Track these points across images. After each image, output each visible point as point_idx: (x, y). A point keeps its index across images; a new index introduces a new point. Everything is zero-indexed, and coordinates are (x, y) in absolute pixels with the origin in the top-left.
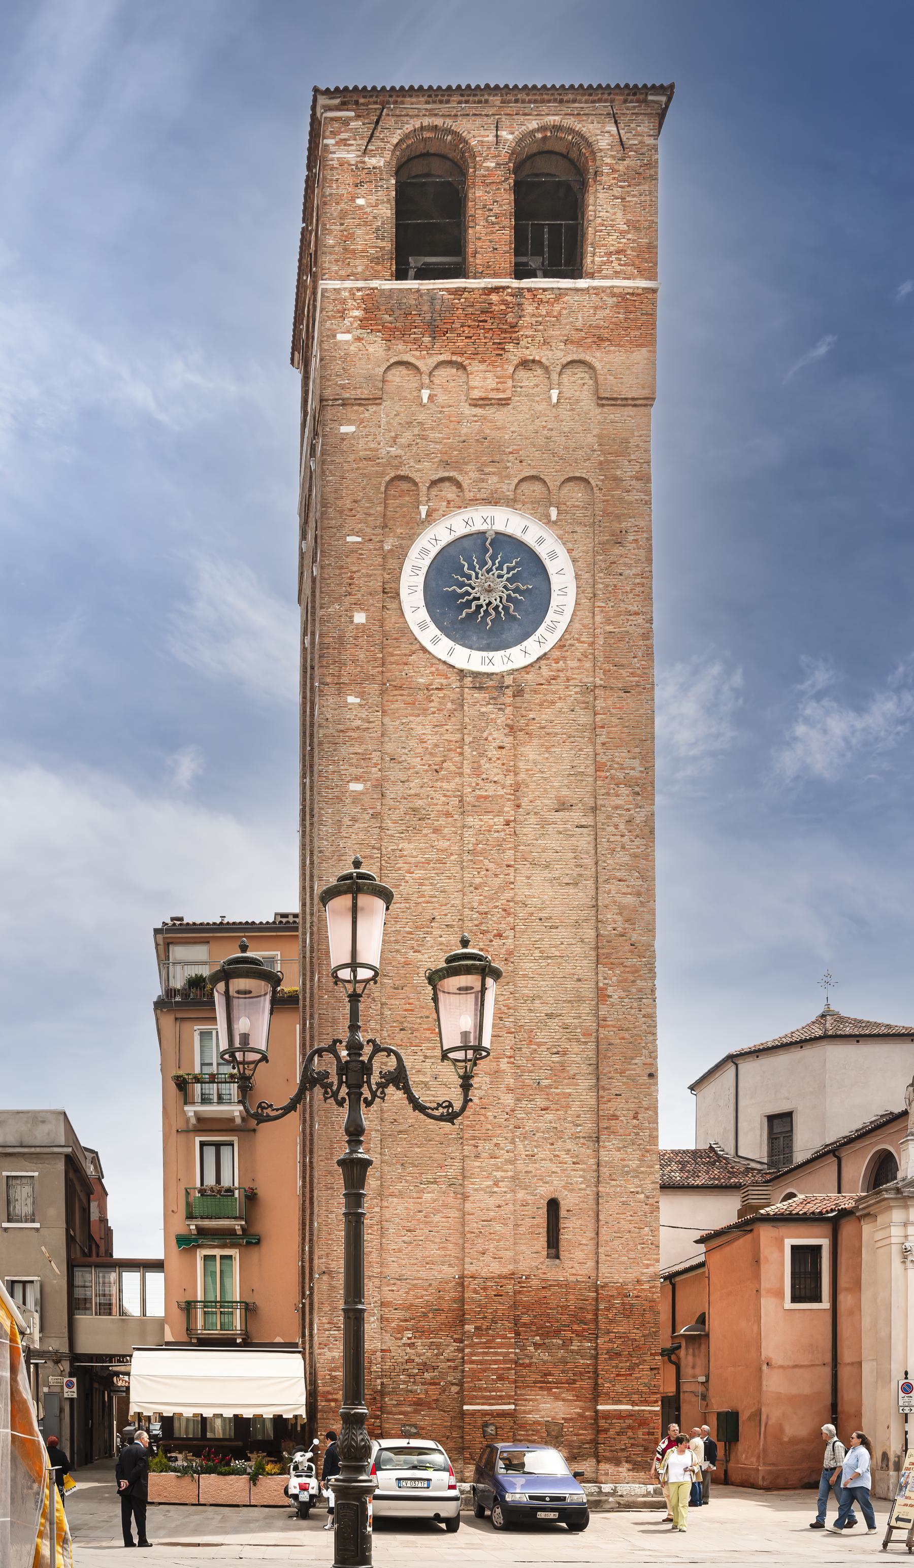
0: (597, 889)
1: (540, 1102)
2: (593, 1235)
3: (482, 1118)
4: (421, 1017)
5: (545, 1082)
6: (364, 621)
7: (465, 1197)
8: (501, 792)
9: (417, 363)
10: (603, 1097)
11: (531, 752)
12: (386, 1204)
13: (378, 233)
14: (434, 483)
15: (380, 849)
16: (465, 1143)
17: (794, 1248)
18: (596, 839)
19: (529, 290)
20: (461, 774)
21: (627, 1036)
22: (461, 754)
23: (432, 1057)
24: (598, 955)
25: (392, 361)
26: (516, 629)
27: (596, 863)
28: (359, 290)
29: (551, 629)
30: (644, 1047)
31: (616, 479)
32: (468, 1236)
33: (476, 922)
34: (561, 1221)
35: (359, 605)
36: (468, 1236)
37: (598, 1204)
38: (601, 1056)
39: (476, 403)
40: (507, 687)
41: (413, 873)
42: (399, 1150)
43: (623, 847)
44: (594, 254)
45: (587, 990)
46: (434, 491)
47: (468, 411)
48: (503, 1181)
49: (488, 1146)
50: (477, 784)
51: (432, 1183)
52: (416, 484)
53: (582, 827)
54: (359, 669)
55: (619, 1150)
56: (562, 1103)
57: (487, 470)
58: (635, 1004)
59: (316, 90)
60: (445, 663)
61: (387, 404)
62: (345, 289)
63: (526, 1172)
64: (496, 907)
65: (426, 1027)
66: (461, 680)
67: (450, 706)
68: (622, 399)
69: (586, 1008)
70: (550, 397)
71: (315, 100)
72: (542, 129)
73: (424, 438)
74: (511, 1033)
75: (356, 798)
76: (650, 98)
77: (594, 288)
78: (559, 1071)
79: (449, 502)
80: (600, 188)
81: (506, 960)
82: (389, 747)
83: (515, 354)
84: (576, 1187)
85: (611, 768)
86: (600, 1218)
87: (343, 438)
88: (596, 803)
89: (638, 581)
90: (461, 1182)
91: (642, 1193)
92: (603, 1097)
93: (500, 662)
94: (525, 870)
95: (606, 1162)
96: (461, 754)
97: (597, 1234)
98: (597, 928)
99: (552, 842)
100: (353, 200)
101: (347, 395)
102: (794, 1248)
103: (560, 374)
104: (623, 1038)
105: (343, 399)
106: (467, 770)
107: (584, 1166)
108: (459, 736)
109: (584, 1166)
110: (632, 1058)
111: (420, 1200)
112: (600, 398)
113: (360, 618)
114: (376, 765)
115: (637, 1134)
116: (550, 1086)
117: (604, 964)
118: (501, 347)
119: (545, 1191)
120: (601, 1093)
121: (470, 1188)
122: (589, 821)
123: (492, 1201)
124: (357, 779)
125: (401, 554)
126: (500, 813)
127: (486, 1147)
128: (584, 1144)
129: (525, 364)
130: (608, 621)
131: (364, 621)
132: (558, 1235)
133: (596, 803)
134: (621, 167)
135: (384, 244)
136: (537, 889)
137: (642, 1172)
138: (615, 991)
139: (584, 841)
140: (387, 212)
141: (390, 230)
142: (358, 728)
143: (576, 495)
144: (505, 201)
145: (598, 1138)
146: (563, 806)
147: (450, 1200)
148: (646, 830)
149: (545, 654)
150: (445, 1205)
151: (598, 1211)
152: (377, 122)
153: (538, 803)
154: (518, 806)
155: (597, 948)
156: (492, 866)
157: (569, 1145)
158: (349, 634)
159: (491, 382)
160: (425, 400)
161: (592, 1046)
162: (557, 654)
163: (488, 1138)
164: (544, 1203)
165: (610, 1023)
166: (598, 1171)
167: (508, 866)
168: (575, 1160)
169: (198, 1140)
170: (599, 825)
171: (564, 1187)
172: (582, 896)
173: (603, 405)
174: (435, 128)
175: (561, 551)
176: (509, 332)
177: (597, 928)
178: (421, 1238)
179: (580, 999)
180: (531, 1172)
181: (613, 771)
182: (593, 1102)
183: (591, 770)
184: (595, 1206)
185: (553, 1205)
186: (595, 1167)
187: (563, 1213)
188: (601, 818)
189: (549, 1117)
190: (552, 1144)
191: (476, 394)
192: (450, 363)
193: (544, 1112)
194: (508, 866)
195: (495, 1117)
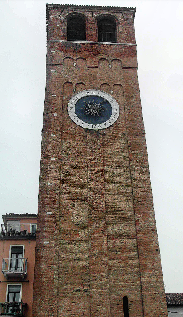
0: (132, 190)
1: (118, 260)
2: (141, 311)
3: (96, 266)
4: (74, 230)
5: (119, 253)
6: (57, 115)
7: (91, 296)
8: (100, 161)
9: (73, 58)
10: (140, 258)
11: (108, 150)
12: (60, 300)
13: (63, 31)
14: (77, 84)
15: (60, 177)
16: (90, 275)
17: (12, 247)
18: (131, 175)
19: (102, 44)
20: (86, 156)
21: (147, 236)
22: (86, 151)
23: (77, 244)
24: (134, 210)
25: (66, 57)
26: (102, 119)
27: (132, 182)
28: (57, 42)
29: (113, 119)
30: (153, 241)
31: (129, 85)
32: (92, 312)
33: (92, 199)
34: (129, 305)
35: (56, 112)
36: (92, 312)
37: (142, 298)
38: (138, 244)
39: (89, 67)
40: (100, 133)
41: (71, 184)
42: (65, 278)
43: (140, 178)
44: (119, 38)
45: (132, 221)
46: (77, 86)
47: (87, 68)
48: (105, 290)
49: (99, 276)
50: (92, 159)
51: (78, 291)
52: (72, 84)
53: (126, 172)
54: (55, 127)
55: (148, 277)
56: (125, 261)
57: (92, 81)
58: (149, 226)
59: (47, 4)
60: (81, 127)
61: (64, 66)
62: (54, 42)
63: (114, 286)
64: (99, 195)
65: (75, 233)
66: (86, 131)
67: (83, 138)
68: (129, 68)
69: (132, 227)
70: (109, 66)
71: (47, 7)
72: (103, 15)
73: (74, 74)
74: (106, 236)
75: (53, 162)
76: (130, 10)
77: (119, 45)
78: (124, 249)
79: (82, 88)
80: (119, 26)
81: (103, 211)
82: (64, 148)
83: (99, 57)
84: (133, 292)
85: (134, 155)
86: (144, 304)
87: (52, 73)
88: (130, 165)
89: (137, 108)
90: (89, 290)
91: (159, 294)
92: (140, 258)
93: (97, 127)
94: (109, 184)
95: (144, 282)
96: (86, 151)
97: (143, 311)
98: (133, 202)
99: (117, 176)
100: (56, 25)
101: (53, 63)
102: (12, 247)
103: (112, 61)
104: (146, 237)
105: (52, 64)
106: (88, 155)
107: (136, 284)
108: (86, 146)
109: (136, 284)
110: (150, 244)
111: (73, 298)
112: (123, 67)
113: (55, 115)
114: (59, 153)
115: (154, 271)
116: (121, 254)
117: (137, 213)
118: (95, 56)
119: (122, 294)
120: (140, 256)
121: (92, 293)
122: (128, 170)
123: (101, 298)
124: (53, 157)
125: (68, 100)
126: (99, 167)
127: (98, 277)
128: (135, 275)
129: (102, 59)
130: (129, 118)
131: (57, 115)
132: (128, 312)
133: (130, 165)
134: (124, 22)
135: (64, 34)
136: (113, 190)
137: (158, 286)
138: (141, 222)
139: (127, 176)
140: (65, 28)
141: (66, 30)
142: (54, 143)
143: (118, 88)
144: (95, 27)
145: (140, 273)
146: (119, 166)
147: (85, 298)
148: (147, 173)
149: (111, 125)
150: (84, 300)
151: (143, 301)
152: (62, 11)
153: (111, 165)
154: (105, 165)
155: (134, 208)
156: (97, 183)
157: (130, 276)
158: (52, 118)
159: (93, 62)
160: (75, 65)
161: (135, 240)
162: (115, 125)
163: (99, 274)
164: (121, 298)
165: (141, 232)
166: (141, 285)
167: (102, 183)
168: (132, 281)
169: (8, 285)
170: (132, 171)
171: (129, 292)
172: (128, 192)
173: (124, 69)
174: (77, 13)
175: (114, 100)
176: (98, 53)
177: (133, 202)
178: (73, 314)
179: (130, 224)
180: (116, 286)
181: (134, 156)
182: (137, 260)
183: (127, 156)
184: (141, 300)
185: (125, 299)
186: (140, 284)
187: (129, 302)
188: (132, 169)
189: (121, 265)
190: (123, 276)
191: (89, 65)
192: (82, 58)
193: (119, 264)
194: (102, 183)
195: (101, 266)
